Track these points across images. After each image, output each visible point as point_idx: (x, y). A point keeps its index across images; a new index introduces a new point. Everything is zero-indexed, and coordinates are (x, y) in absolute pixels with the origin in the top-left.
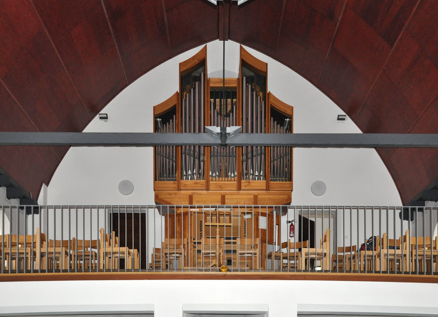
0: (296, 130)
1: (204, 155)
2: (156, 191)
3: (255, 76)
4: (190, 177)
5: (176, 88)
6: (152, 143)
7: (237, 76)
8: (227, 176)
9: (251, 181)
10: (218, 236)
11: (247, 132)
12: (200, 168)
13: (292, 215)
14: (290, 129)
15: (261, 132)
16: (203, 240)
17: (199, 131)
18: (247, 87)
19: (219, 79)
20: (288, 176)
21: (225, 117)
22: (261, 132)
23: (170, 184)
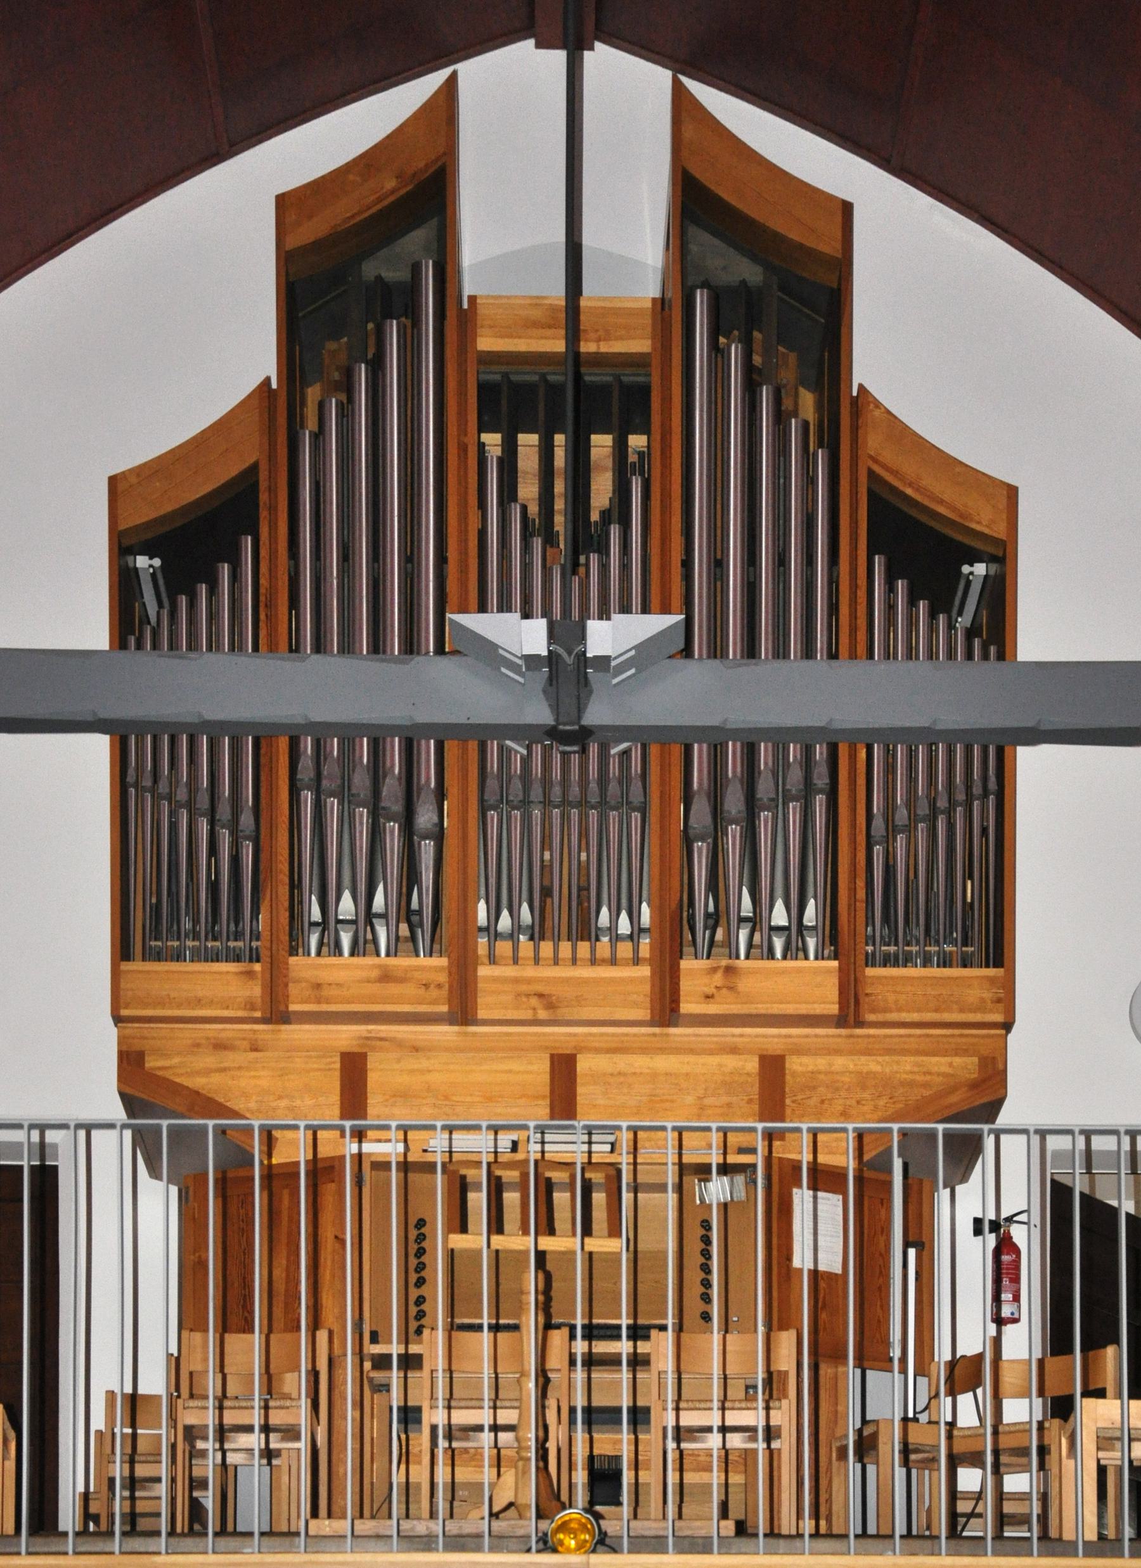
0: (1038, 637)
1: (441, 794)
2: (132, 1028)
3: (769, 287)
4: (346, 939)
5: (256, 358)
6: (104, 714)
7: (651, 289)
8: (585, 930)
9: (742, 962)
10: (530, 1321)
11: (717, 650)
12: (411, 876)
13: (1008, 1183)
14: (994, 629)
15: (808, 652)
16: (433, 1345)
17: (411, 646)
18: (717, 352)
19: (536, 302)
20: (986, 934)
21: (576, 551)
22: (808, 652)
23: (219, 984)
